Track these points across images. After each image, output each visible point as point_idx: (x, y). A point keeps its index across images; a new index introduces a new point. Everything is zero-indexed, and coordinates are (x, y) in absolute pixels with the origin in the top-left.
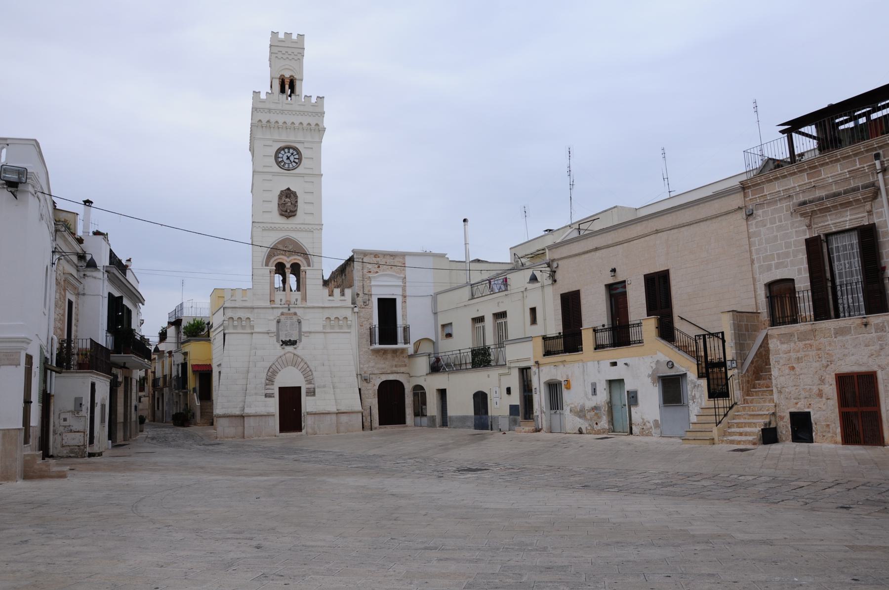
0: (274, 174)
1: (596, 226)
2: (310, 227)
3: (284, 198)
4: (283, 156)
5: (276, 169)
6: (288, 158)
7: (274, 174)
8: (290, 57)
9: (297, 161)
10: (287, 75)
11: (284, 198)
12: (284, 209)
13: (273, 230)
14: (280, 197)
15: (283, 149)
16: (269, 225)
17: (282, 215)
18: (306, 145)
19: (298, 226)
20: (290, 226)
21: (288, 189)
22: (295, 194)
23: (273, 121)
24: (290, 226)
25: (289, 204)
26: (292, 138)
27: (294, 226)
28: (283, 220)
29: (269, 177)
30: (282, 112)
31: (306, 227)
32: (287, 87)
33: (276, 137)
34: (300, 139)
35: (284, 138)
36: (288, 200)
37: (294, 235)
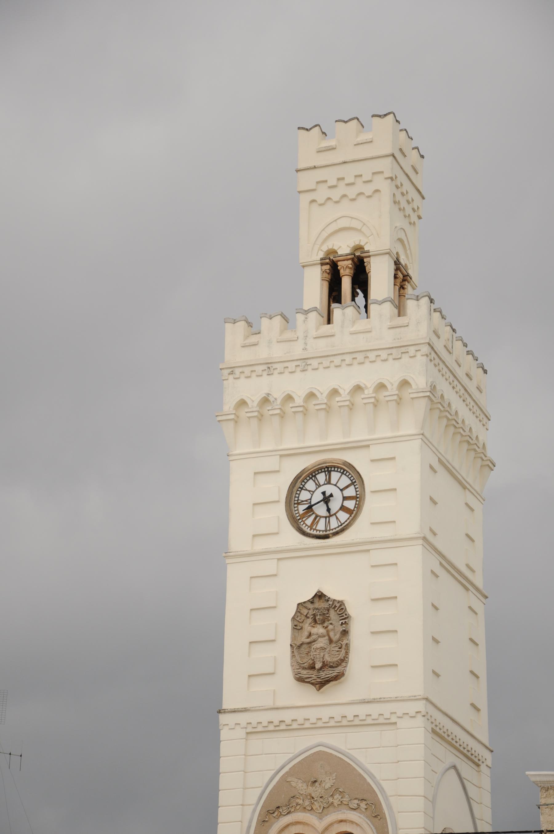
0: (283, 555)
1: (253, 709)
2: (386, 709)
3: (307, 627)
4: (312, 493)
5: (291, 537)
6: (326, 499)
7: (283, 555)
8: (336, 195)
9: (350, 504)
10: (344, 246)
11: (307, 627)
12: (307, 661)
13: (351, 726)
14: (297, 627)
15: (310, 475)
16: (264, 717)
17: (301, 680)
18: (376, 452)
19: (350, 711)
20: (325, 713)
21: (320, 596)
22: (340, 607)
23: (278, 395)
24: (325, 713)
25: (322, 643)
26: (335, 438)
27: (337, 712)
28: (307, 695)
29: (268, 566)
30: (304, 364)
31: (374, 710)
32: (346, 284)
33: (291, 443)
34: (359, 434)
35: (313, 441)
36: (319, 630)
37: (339, 742)
